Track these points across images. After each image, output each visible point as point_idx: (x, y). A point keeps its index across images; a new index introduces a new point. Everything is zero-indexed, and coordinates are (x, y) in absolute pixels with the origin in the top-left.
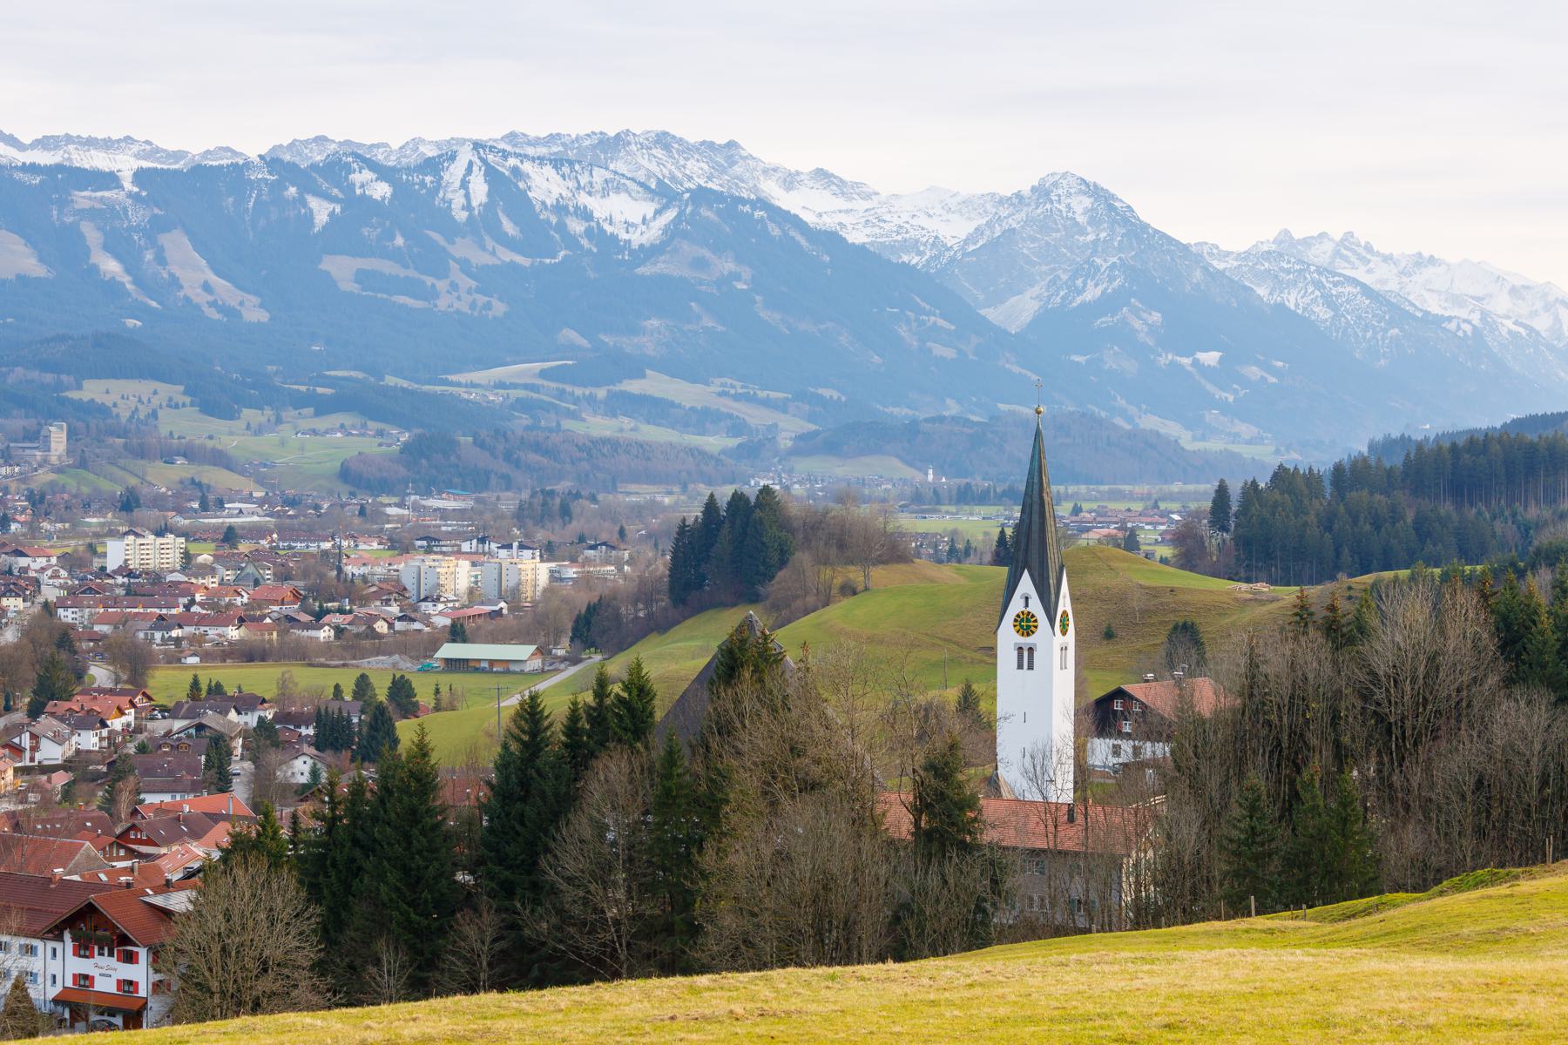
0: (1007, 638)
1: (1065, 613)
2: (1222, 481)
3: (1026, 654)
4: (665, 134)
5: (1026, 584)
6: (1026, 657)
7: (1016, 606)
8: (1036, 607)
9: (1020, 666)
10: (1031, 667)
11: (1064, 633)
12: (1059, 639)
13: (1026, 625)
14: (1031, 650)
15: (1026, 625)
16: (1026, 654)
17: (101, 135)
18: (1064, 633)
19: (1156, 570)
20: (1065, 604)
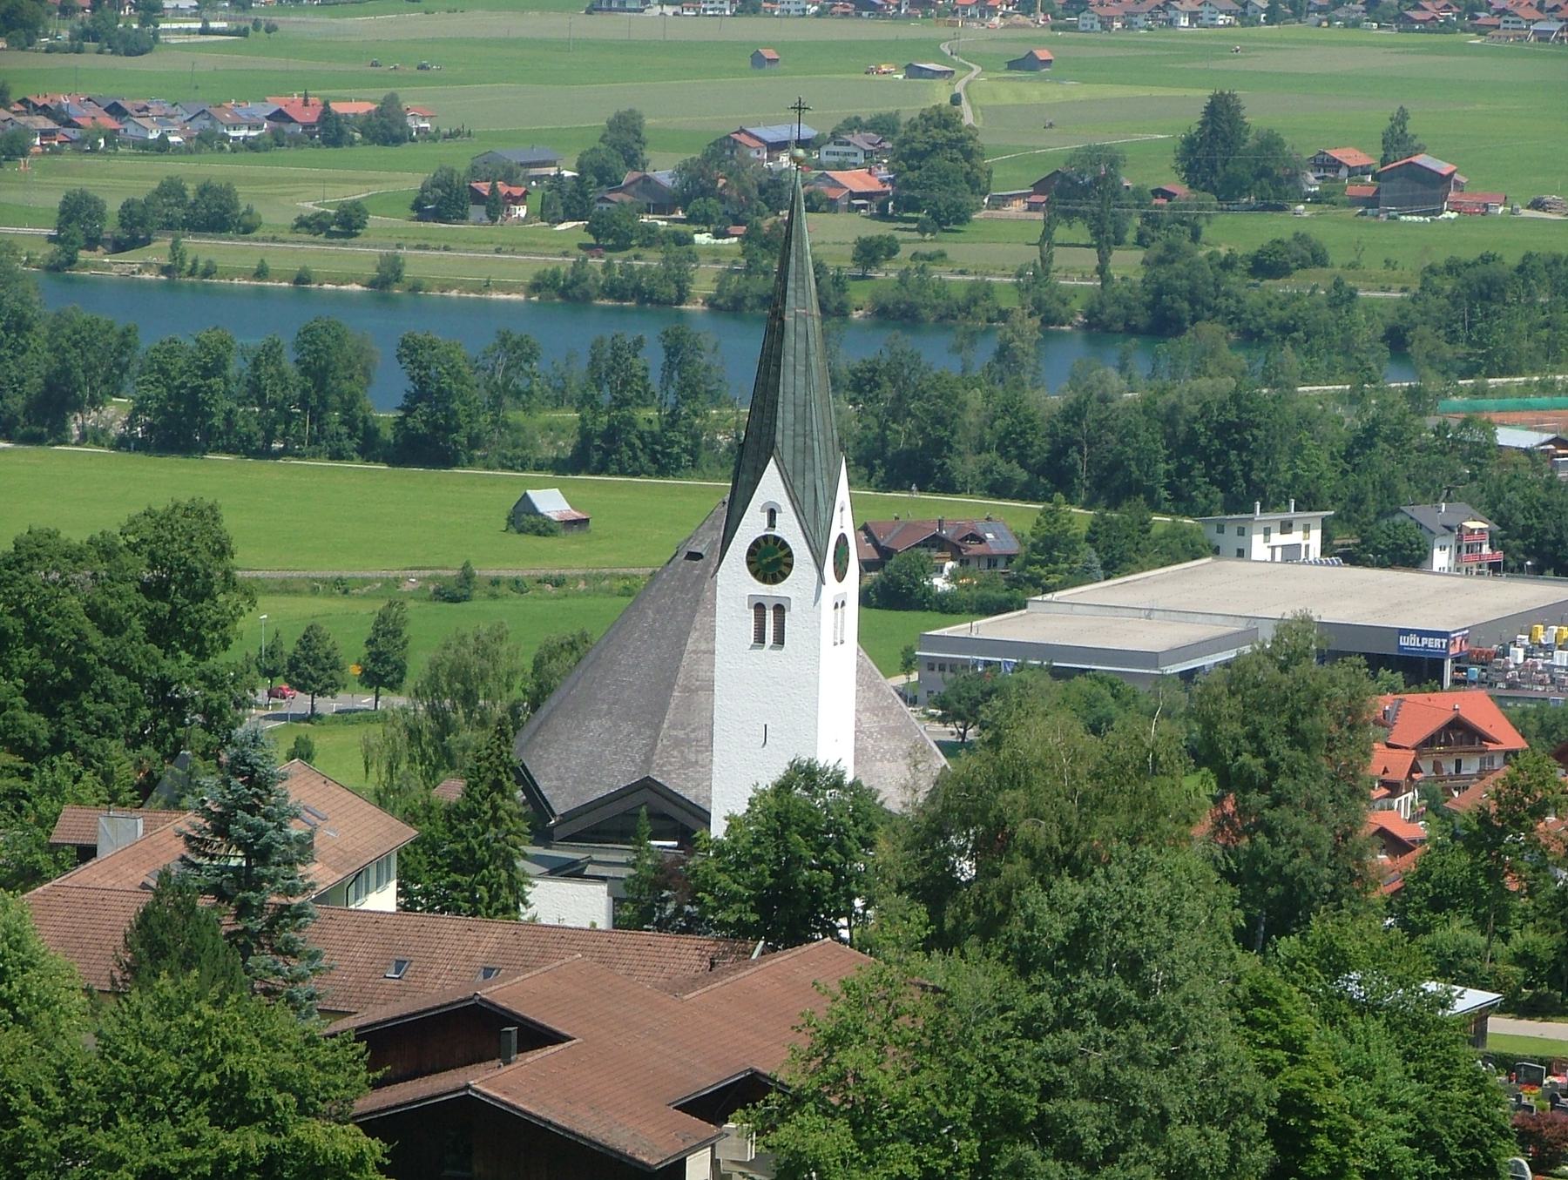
0: (734, 582)
1: (842, 539)
2: (466, 566)
3: (770, 615)
4: (619, 116)
5: (771, 487)
6: (770, 624)
7: (752, 526)
8: (789, 529)
9: (760, 638)
10: (780, 640)
11: (840, 575)
12: (832, 587)
13: (770, 560)
14: (780, 610)
15: (770, 560)
16: (770, 615)
17: (56, 55)
18: (840, 575)
19: (748, 185)
20: (843, 523)
